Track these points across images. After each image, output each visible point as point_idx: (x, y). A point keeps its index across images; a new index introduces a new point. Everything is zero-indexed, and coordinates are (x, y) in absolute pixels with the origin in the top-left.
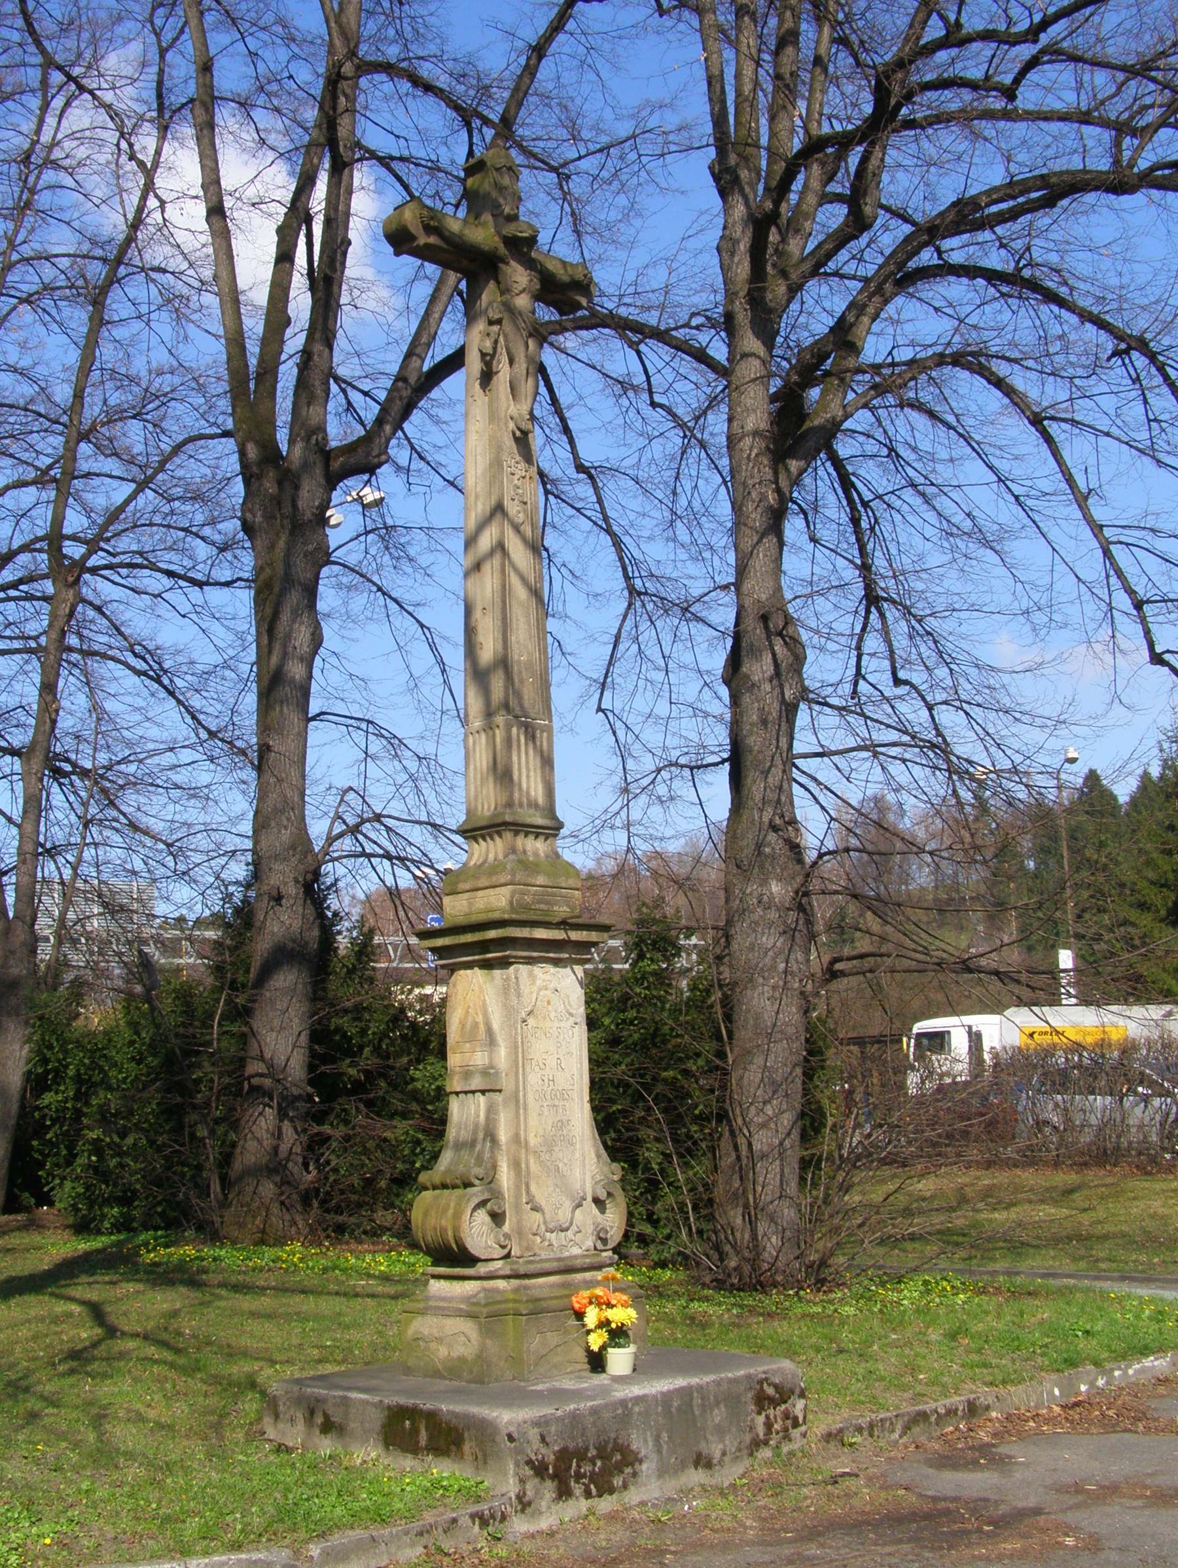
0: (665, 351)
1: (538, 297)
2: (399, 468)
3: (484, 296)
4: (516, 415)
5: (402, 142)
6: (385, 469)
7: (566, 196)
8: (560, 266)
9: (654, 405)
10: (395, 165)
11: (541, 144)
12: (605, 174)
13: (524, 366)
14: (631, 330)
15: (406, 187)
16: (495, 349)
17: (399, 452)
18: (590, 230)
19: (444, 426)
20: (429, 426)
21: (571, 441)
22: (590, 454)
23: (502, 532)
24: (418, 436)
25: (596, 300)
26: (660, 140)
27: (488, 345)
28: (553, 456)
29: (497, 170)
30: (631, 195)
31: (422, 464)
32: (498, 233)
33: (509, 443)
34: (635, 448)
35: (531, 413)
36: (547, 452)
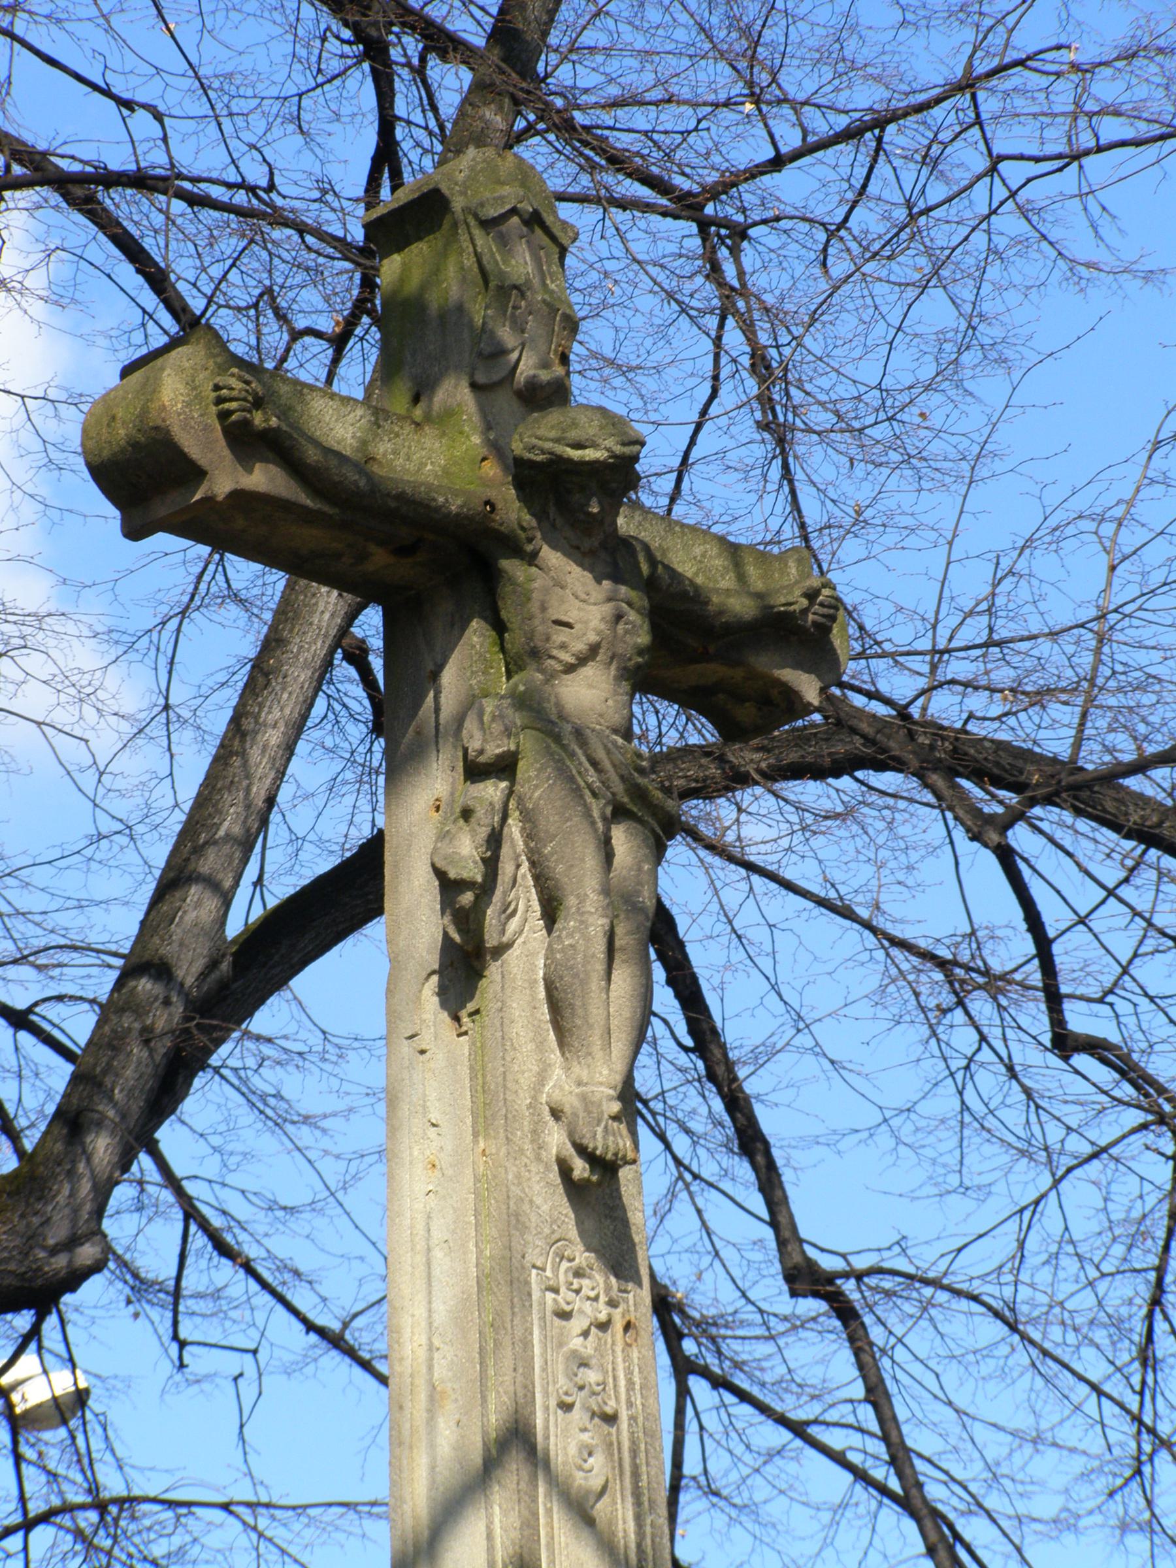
0: (1103, 850)
1: (644, 679)
2: (140, 1287)
3: (448, 676)
4: (570, 1103)
5: (142, 121)
6: (95, 1291)
7: (733, 300)
8: (719, 562)
9: (1065, 1044)
10: (117, 201)
11: (640, 118)
12: (868, 221)
13: (597, 925)
14: (979, 775)
15: (158, 279)
16: (491, 864)
17: (139, 1228)
18: (821, 418)
19: (304, 1135)
20: (252, 1133)
21: (769, 1181)
22: (834, 1229)
23: (530, 1524)
24: (211, 1168)
25: (851, 669)
26: (1064, 95)
27: (466, 854)
28: (708, 1242)
29: (487, 224)
30: (966, 293)
31: (226, 1271)
32: (497, 449)
33: (549, 1205)
34: (998, 1207)
35: (628, 1094)
36: (683, 1219)
